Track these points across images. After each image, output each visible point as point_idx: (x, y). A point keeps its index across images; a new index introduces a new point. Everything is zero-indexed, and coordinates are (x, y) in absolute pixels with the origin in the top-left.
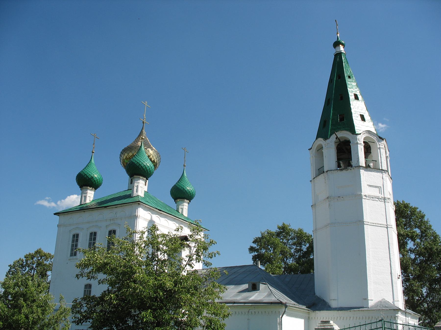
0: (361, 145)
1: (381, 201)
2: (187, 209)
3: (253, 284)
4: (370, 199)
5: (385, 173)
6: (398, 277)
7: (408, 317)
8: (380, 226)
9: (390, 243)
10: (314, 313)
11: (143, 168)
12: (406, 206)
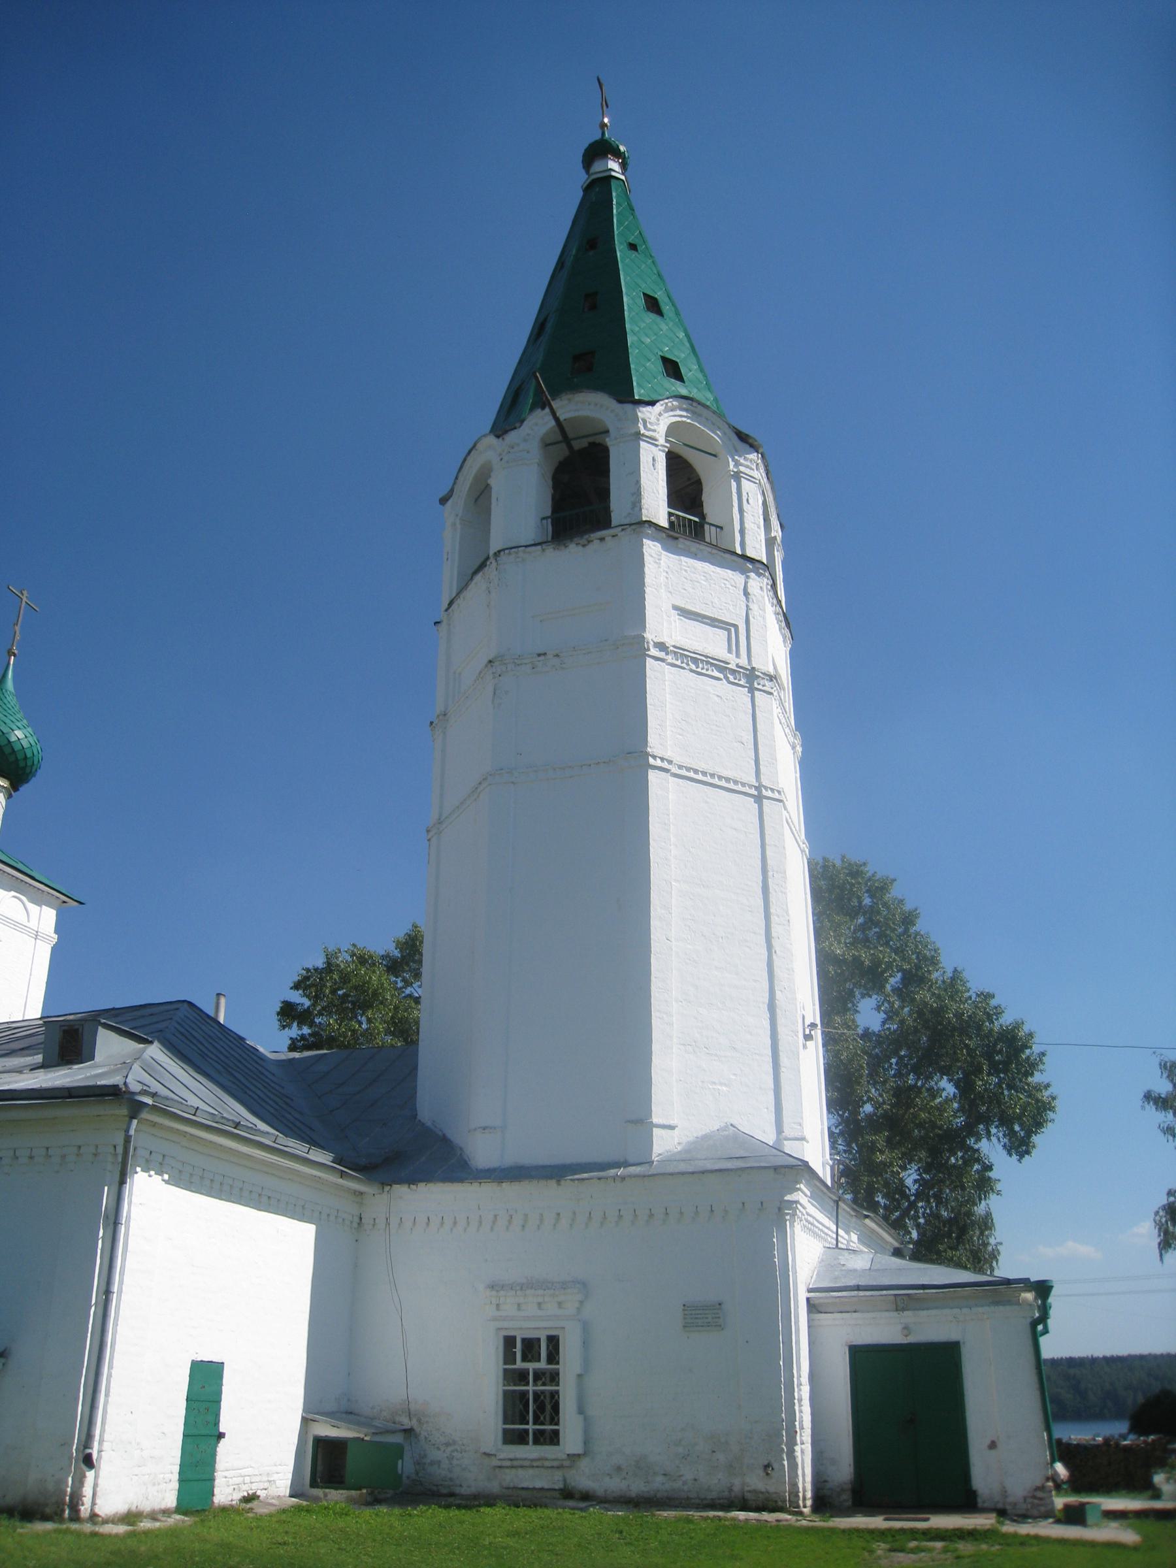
0: (656, 446)
1: (736, 681)
3: (65, 1031)
4: (684, 665)
5: (759, 575)
6: (807, 1032)
7: (847, 1232)
8: (729, 786)
9: (769, 868)
10: (385, 1196)
12: (855, 871)
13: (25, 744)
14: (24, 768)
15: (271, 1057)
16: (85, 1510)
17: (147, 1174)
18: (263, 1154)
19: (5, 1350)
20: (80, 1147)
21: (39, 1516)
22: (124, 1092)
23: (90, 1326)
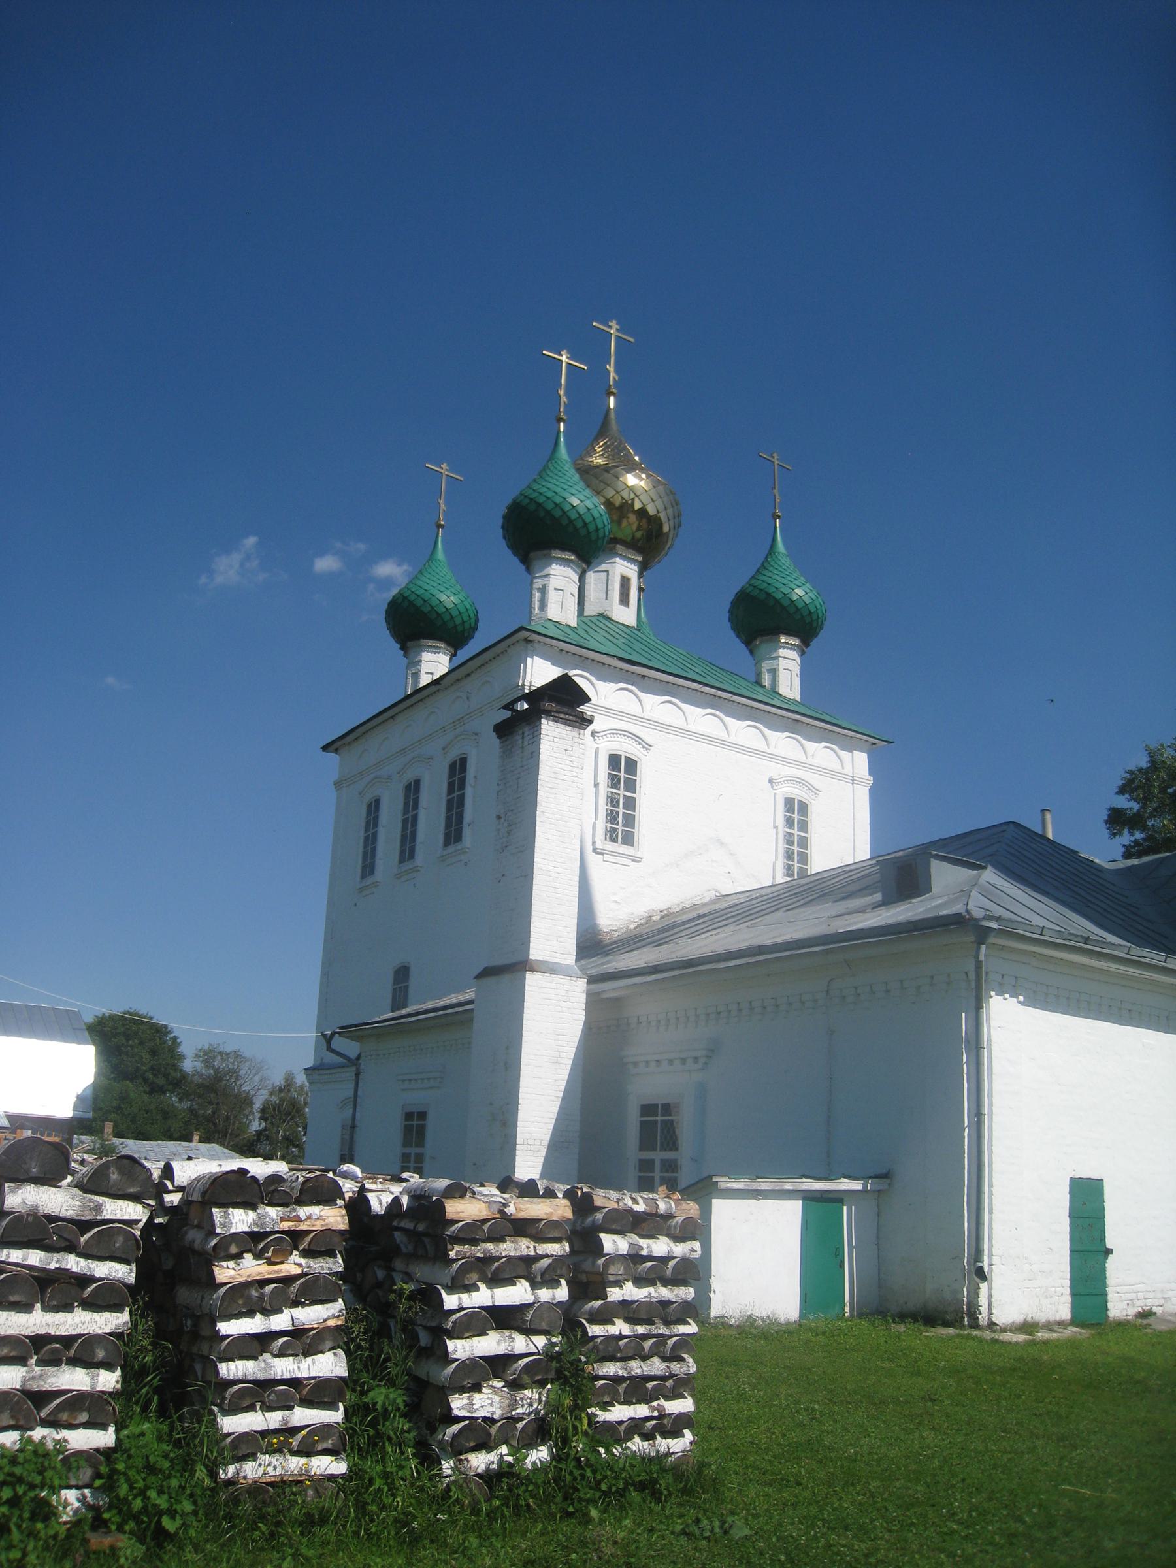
13: (807, 599)
14: (811, 623)
15: (1108, 867)
16: (983, 1318)
17: (1001, 998)
18: (1117, 966)
19: (889, 1171)
20: (932, 977)
21: (940, 1322)
22: (968, 919)
23: (966, 1147)
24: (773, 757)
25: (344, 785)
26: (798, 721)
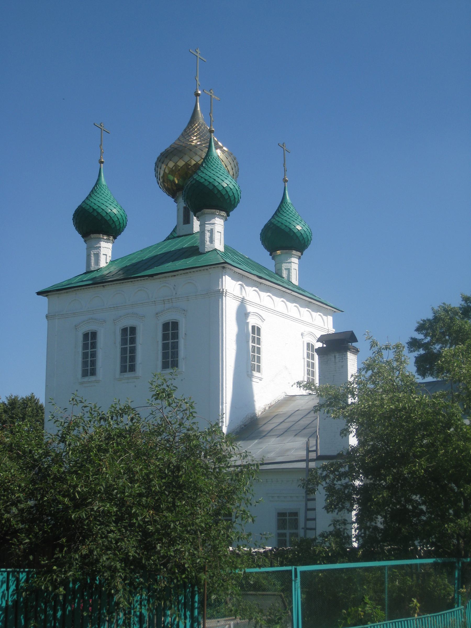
2: (297, 269)
11: (221, 194)
24: (303, 322)
25: (57, 318)
26: (310, 302)
